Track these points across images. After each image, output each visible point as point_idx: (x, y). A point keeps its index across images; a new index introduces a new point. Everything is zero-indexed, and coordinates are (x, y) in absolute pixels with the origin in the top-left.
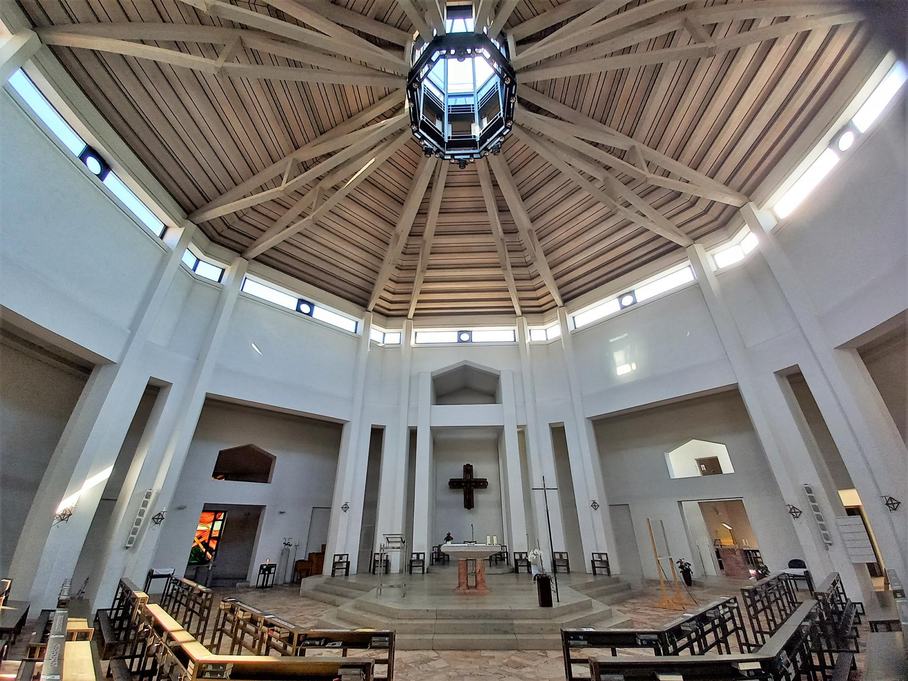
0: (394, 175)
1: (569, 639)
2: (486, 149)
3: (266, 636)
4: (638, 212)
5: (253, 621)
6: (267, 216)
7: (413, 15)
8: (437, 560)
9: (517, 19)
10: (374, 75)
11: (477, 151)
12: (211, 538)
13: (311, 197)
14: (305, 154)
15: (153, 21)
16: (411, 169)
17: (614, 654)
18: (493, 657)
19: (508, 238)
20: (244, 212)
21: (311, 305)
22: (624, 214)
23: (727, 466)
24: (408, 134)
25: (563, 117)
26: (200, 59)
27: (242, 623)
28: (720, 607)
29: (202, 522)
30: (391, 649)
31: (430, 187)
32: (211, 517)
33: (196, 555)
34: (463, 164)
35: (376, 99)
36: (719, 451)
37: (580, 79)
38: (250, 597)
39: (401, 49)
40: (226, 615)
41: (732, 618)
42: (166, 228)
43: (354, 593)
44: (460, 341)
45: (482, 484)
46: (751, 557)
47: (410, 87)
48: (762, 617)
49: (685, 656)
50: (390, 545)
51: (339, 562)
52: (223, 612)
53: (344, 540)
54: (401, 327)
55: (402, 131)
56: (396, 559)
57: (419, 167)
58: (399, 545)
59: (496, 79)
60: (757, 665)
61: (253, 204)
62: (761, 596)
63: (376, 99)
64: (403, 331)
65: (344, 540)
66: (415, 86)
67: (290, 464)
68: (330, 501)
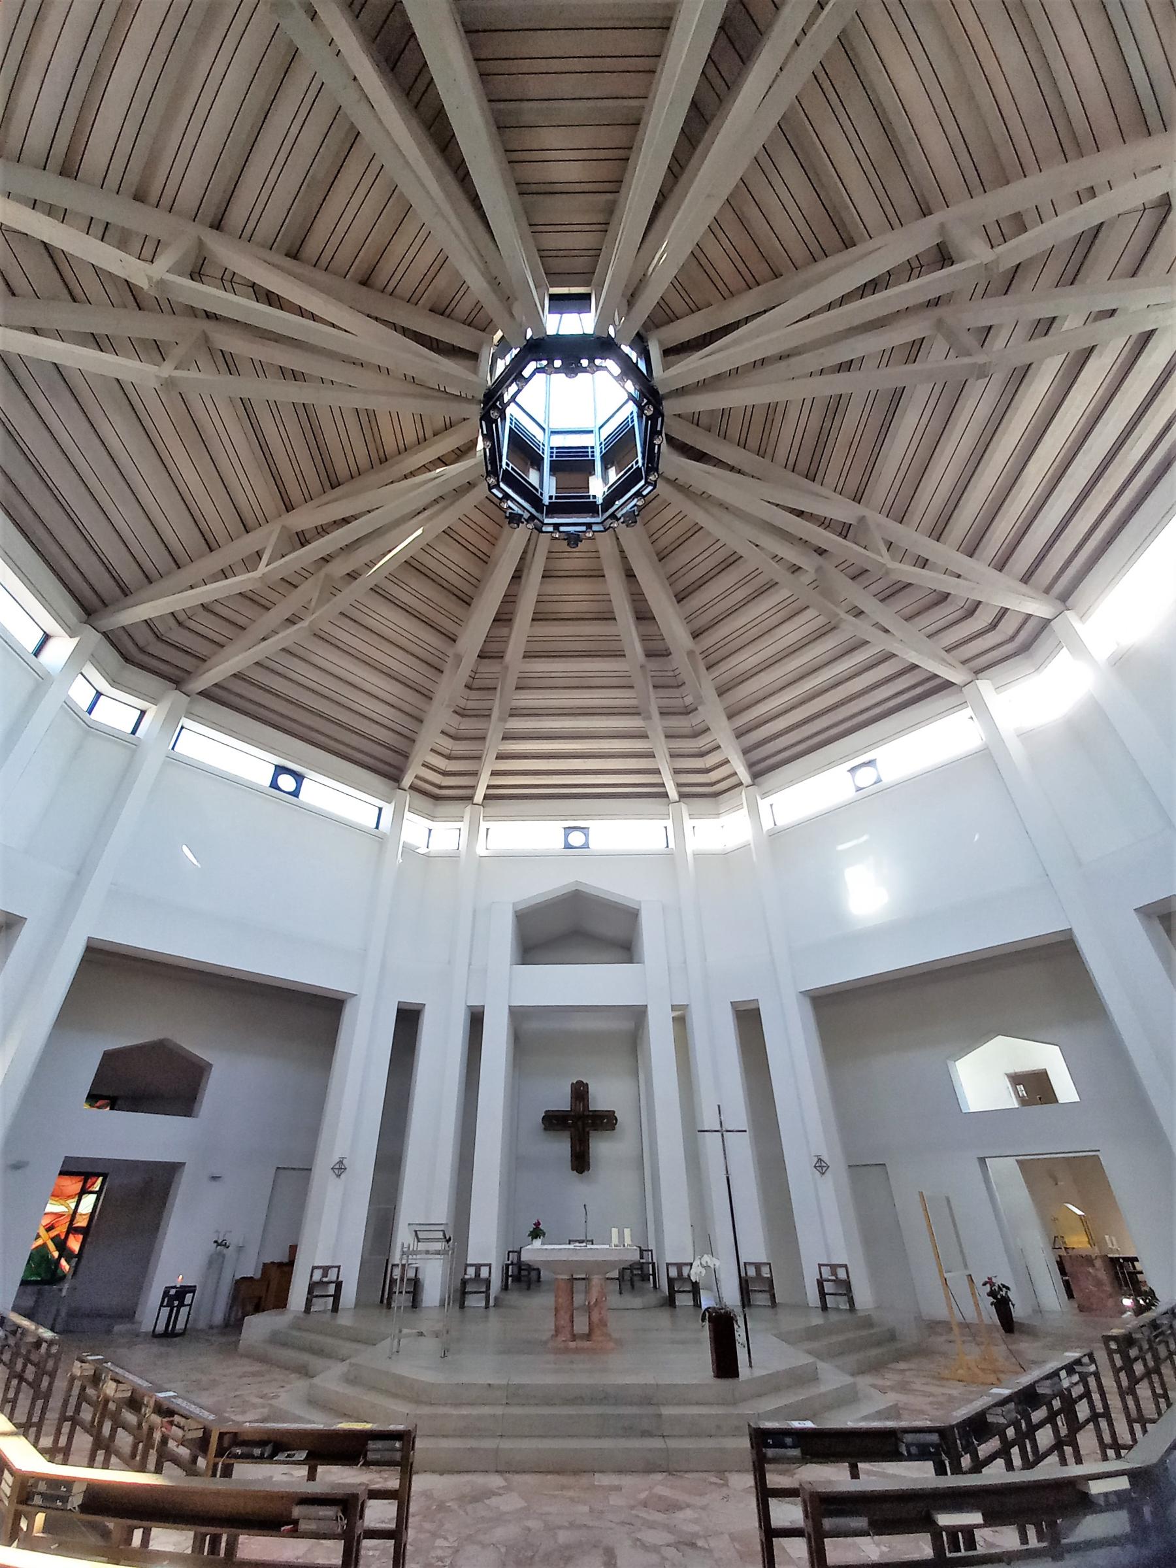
0: (455, 554)
1: (766, 1443)
2: (613, 516)
3: (157, 1436)
4: (876, 625)
5: (134, 1403)
6: (228, 620)
7: (492, 306)
8: (517, 1279)
9: (663, 316)
10: (427, 397)
11: (599, 520)
12: (72, 1230)
13: (309, 589)
14: (303, 519)
15: (55, 298)
16: (485, 547)
17: (855, 1475)
18: (618, 1488)
19: (654, 664)
20: (190, 614)
21: (299, 778)
22: (851, 628)
23: (1065, 1089)
24: (481, 491)
25: (745, 468)
26: (134, 364)
27: (112, 1406)
28: (1063, 1373)
29: (58, 1195)
30: (407, 1469)
31: (517, 576)
32: (74, 1185)
33: (39, 1265)
34: (574, 540)
35: (429, 434)
36: (1047, 1057)
37: (771, 408)
38: (141, 1354)
39: (473, 356)
40: (83, 1388)
41: (1087, 1394)
42: (47, 637)
43: (346, 1347)
44: (568, 846)
45: (606, 1121)
46: (1125, 1274)
47: (485, 417)
48: (1143, 1390)
49: (995, 1474)
50: (422, 1246)
51: (321, 1283)
52: (77, 1384)
53: (333, 1238)
54: (461, 819)
55: (471, 485)
56: (435, 1278)
57: (500, 543)
58: (438, 1246)
59: (631, 407)
60: (1123, 1483)
61: (205, 600)
62: (1141, 1349)
63: (429, 434)
64: (464, 826)
65: (333, 1238)
66: (494, 414)
67: (239, 1076)
68: (311, 1154)
